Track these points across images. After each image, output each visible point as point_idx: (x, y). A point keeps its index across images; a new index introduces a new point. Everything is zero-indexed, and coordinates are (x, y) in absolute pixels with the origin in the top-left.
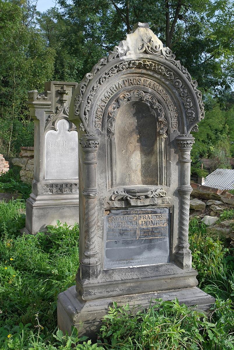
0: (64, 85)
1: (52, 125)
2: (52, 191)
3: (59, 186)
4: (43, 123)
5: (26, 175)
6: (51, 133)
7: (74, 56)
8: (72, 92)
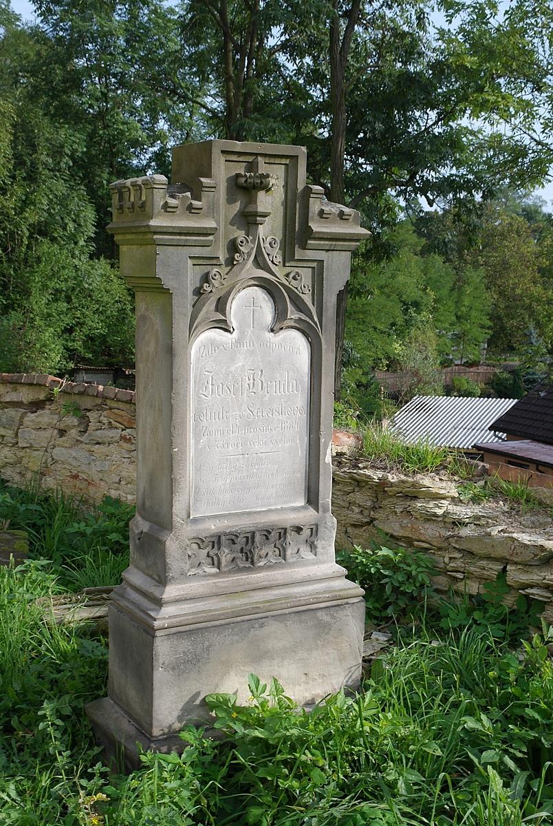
0: (257, 155)
1: (217, 310)
2: (216, 562)
3: (241, 541)
4: (183, 304)
5: (19, 461)
6: (212, 343)
7: (61, 121)
8: (283, 184)
